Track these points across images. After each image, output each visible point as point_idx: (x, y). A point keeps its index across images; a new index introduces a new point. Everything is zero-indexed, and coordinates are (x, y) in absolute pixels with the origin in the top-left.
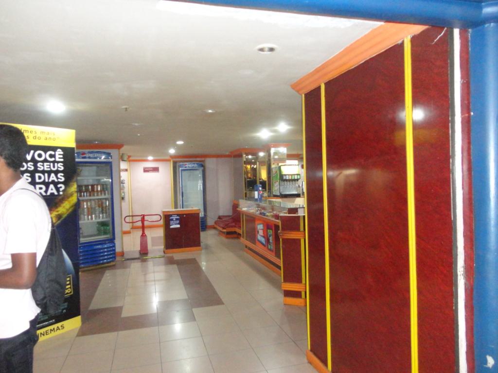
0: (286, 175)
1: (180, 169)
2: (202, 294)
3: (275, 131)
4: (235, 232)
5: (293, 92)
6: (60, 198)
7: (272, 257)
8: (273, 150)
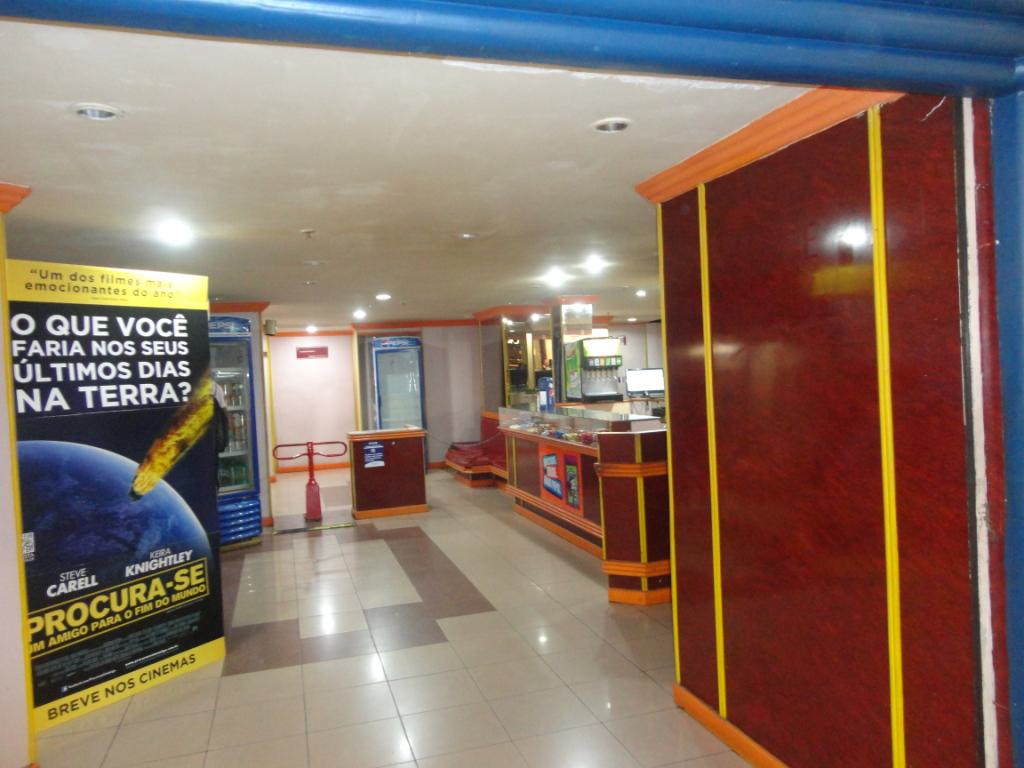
0: (593, 358)
1: (374, 350)
2: (441, 600)
3: (580, 272)
4: (489, 476)
5: (638, 198)
6: (184, 408)
7: (576, 518)
8: (565, 309)
